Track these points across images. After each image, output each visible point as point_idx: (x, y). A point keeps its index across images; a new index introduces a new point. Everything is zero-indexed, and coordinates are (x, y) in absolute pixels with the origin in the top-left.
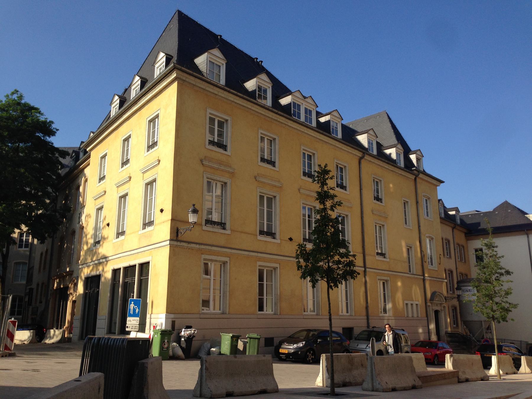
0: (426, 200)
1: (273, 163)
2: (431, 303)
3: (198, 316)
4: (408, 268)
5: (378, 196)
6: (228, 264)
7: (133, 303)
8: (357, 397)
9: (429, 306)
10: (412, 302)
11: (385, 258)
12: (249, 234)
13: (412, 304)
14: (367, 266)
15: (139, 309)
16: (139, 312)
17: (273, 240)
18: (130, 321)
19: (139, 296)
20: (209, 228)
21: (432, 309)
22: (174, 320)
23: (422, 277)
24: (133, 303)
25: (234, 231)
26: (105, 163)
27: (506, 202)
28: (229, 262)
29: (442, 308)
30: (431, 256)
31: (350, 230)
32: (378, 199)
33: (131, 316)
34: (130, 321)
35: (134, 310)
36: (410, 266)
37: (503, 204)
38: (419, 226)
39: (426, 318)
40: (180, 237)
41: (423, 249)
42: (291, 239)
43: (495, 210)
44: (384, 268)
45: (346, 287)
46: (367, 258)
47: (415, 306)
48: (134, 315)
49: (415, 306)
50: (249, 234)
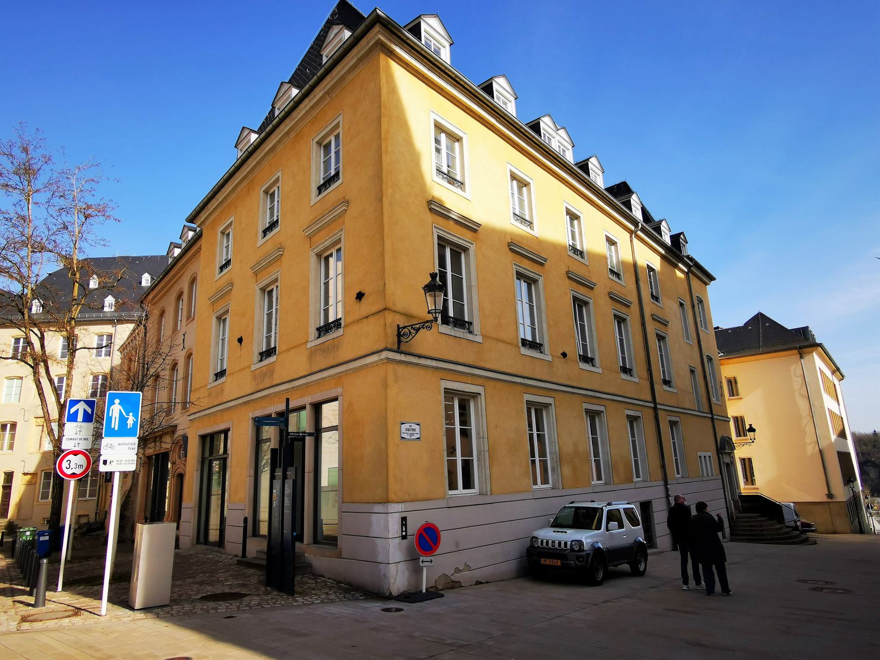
1: (461, 185)
3: (443, 503)
6: (483, 398)
7: (117, 401)
8: (39, 394)
15: (136, 416)
16: (135, 424)
18: (111, 446)
22: (404, 515)
24: (117, 401)
26: (627, 331)
27: (760, 319)
28: (483, 394)
33: (112, 433)
34: (111, 446)
35: (123, 420)
38: (699, 342)
42: (564, 355)
43: (747, 324)
45: (326, 311)
48: (123, 431)
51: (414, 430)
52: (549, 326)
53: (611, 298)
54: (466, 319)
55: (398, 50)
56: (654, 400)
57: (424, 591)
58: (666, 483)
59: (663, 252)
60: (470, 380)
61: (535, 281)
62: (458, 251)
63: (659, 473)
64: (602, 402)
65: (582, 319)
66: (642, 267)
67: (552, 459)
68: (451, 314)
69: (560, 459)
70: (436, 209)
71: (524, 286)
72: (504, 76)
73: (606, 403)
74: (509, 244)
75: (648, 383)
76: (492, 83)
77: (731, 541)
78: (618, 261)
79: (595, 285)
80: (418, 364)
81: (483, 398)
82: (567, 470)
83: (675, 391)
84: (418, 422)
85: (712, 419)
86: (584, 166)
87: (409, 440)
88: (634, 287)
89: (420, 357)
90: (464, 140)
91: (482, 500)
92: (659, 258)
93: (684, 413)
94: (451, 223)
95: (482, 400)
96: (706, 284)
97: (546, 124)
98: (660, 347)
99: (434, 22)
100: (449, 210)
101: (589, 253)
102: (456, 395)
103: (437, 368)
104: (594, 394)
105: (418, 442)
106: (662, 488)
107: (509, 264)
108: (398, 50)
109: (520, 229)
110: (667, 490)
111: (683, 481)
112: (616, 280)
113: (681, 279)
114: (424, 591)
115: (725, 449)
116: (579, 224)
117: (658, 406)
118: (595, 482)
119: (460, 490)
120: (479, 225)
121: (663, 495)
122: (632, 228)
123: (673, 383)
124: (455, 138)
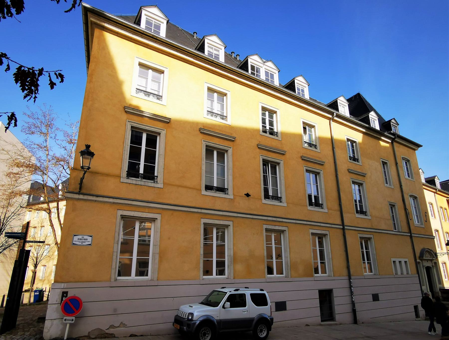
0: (406, 163)
2: (421, 260)
4: (393, 226)
5: (354, 156)
6: (287, 232)
9: (419, 263)
10: (400, 260)
11: (366, 215)
12: (190, 188)
13: (400, 262)
14: (345, 224)
17: (321, 210)
19: (368, 260)
20: (209, 193)
21: (423, 266)
23: (409, 234)
25: (197, 190)
26: (320, 180)
29: (433, 264)
30: (360, 201)
31: (323, 187)
32: (354, 159)
36: (394, 224)
37: (355, 96)
38: (401, 186)
39: (417, 275)
40: (83, 191)
41: (407, 207)
42: (248, 195)
44: (365, 226)
46: (344, 215)
47: (403, 263)
49: (403, 263)
50: (190, 188)
51: (86, 239)
52: (234, 178)
53: (302, 159)
54: (226, 187)
55: (107, 25)
56: (343, 224)
57: (65, 338)
58: (350, 278)
59: (364, 130)
60: (147, 210)
61: (319, 173)
62: (274, 166)
63: (345, 272)
64: (285, 224)
65: (317, 183)
66: (341, 142)
67: (228, 259)
68: (359, 209)
69: (235, 260)
70: (134, 112)
71: (357, 187)
72: (343, 96)
73: (288, 225)
74: (301, 157)
75: (339, 213)
76: (337, 101)
77: (425, 320)
78: (316, 137)
79: (235, 138)
80: (96, 201)
81: (287, 232)
82: (240, 267)
83: (370, 218)
84: (90, 235)
85: (411, 237)
86: (291, 86)
87: (79, 245)
88: (331, 153)
89: (97, 196)
90: (278, 113)
91: (375, 277)
92: (361, 135)
93: (379, 232)
94: (146, 119)
95: (231, 228)
96: (415, 150)
97: (254, 60)
98: (359, 190)
99: (256, 58)
100: (142, 112)
101: (282, 133)
102: (215, 226)
103: (114, 203)
104: (276, 219)
105: (90, 246)
106: (347, 282)
107: (302, 167)
108: (107, 25)
109: (218, 121)
110: (350, 282)
111: (375, 277)
112: (315, 149)
113: (385, 147)
114: (65, 338)
115: (423, 257)
116: (277, 116)
117: (413, 235)
118: (368, 273)
119: (320, 274)
120: (170, 119)
121: (347, 285)
122: (331, 116)
123: (368, 213)
124: (222, 95)
